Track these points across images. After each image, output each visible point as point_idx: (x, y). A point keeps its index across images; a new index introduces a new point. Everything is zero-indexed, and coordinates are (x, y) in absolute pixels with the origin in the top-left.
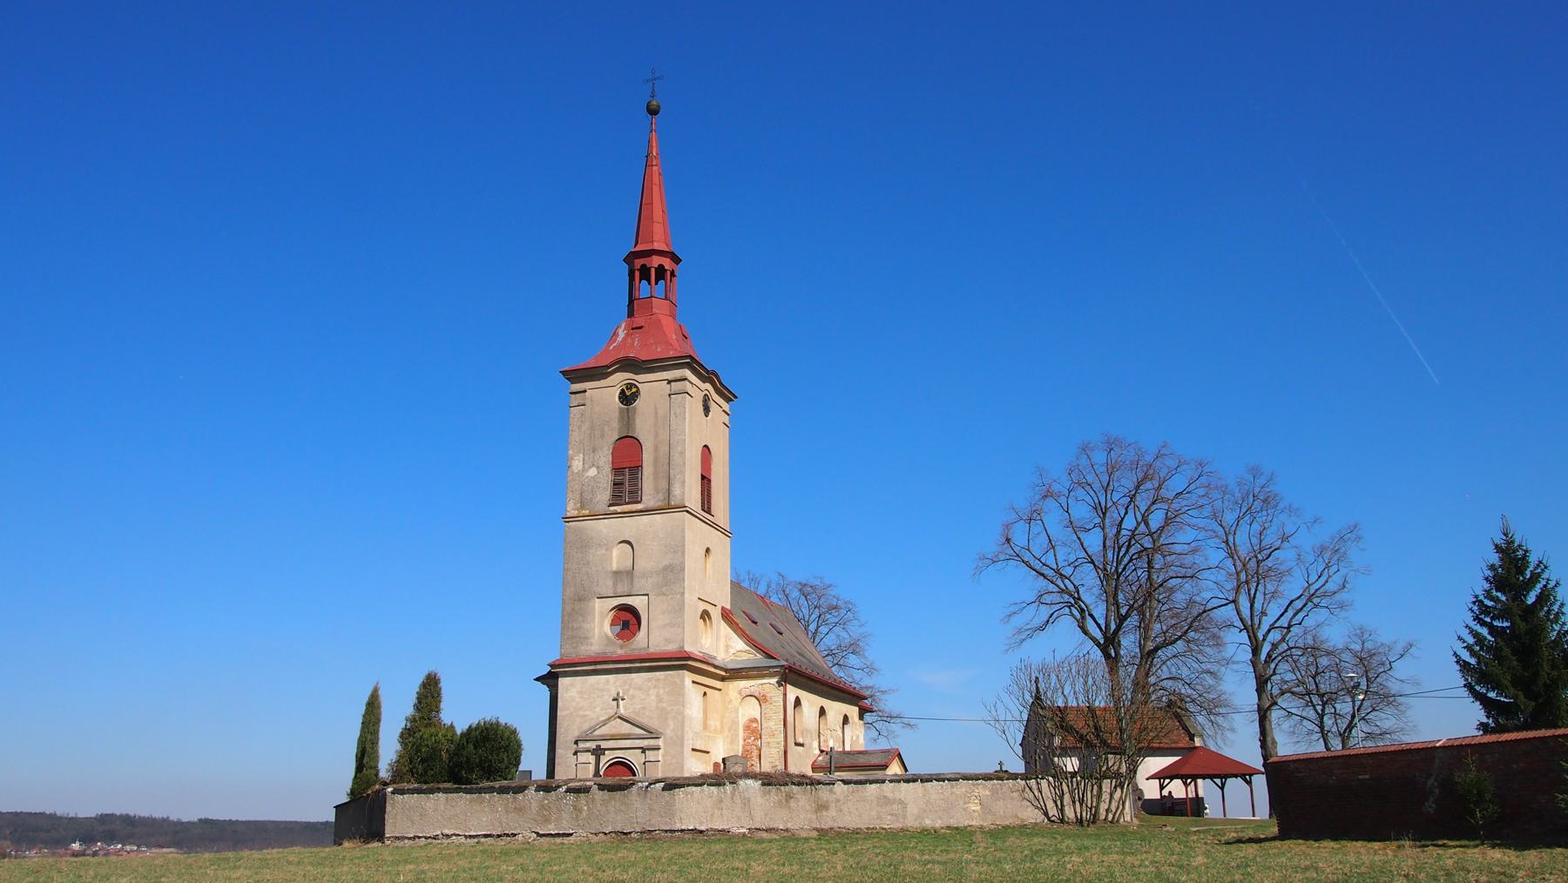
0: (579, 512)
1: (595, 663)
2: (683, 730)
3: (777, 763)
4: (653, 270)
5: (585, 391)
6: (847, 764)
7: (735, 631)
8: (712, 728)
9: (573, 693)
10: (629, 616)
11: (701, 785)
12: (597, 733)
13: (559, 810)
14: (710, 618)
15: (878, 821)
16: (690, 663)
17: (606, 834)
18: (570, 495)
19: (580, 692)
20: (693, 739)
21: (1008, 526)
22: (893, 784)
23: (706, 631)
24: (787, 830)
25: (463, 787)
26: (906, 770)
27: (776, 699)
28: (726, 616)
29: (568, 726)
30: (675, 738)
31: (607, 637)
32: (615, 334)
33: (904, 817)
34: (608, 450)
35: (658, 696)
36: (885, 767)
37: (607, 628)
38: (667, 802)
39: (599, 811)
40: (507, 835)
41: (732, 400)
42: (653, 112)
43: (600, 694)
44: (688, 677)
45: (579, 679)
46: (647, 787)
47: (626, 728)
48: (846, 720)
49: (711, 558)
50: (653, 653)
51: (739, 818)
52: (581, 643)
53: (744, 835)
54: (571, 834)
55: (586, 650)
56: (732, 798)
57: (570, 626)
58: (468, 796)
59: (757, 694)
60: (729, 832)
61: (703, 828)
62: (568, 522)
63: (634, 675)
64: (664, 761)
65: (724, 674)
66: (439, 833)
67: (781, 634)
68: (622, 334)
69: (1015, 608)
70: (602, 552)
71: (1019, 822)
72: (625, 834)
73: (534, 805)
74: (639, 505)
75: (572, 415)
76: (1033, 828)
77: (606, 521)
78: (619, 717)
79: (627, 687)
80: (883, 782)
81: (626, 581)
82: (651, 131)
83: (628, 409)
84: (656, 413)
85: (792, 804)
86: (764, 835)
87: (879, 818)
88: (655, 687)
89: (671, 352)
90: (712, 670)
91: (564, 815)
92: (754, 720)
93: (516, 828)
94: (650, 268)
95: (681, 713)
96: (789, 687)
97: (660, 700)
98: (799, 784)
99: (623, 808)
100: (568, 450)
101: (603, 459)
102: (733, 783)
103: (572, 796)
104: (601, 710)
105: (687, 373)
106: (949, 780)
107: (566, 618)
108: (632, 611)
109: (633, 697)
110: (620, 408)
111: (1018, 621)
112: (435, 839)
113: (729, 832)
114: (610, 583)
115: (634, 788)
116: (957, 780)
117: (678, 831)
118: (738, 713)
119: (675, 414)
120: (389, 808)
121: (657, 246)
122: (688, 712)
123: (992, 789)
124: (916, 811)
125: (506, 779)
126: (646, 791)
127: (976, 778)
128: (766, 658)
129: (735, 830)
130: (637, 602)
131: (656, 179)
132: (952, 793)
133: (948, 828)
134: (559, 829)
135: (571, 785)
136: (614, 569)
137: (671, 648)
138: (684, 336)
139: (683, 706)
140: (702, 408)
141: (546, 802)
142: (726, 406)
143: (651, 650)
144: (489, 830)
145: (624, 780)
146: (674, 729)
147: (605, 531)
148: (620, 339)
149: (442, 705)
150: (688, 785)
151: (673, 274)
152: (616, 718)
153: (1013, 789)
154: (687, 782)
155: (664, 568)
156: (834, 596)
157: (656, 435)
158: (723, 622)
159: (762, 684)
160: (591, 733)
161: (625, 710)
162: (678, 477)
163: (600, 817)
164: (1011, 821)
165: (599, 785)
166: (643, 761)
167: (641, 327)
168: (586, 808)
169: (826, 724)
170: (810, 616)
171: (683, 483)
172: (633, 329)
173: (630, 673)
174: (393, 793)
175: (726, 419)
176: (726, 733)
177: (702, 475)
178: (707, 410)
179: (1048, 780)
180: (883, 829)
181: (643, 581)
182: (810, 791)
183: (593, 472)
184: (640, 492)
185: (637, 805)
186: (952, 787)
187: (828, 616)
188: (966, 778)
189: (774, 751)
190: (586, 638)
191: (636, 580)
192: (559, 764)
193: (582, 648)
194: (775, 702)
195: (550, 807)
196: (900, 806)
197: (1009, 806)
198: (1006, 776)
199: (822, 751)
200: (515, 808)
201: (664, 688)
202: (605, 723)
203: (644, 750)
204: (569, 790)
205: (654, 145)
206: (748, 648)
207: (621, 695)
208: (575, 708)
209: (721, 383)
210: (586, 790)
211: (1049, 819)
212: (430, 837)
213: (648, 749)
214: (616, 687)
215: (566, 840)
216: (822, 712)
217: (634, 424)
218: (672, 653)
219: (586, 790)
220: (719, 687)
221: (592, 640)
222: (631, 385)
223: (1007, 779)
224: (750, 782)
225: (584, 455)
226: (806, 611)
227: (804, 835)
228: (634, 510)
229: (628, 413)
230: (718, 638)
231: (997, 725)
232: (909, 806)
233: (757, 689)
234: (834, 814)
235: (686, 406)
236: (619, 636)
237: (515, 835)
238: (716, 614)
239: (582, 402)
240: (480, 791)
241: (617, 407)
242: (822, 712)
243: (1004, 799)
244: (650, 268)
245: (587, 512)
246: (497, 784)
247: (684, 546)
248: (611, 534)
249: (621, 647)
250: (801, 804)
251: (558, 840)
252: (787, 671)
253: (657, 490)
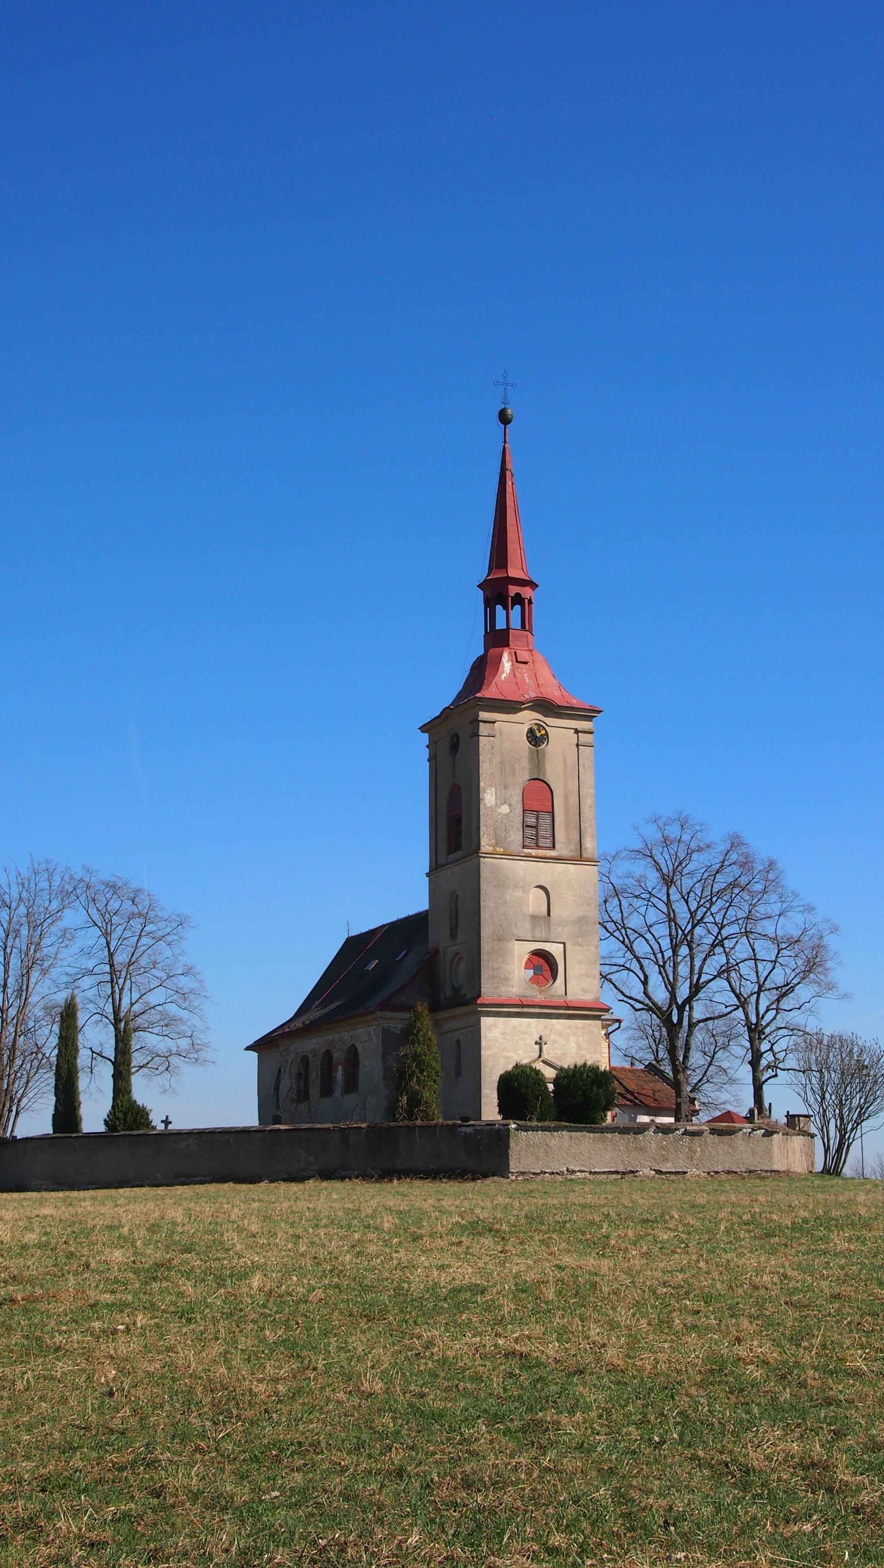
0: (495, 849)
1: (523, 1006)
5: (494, 722)
19: (503, 1033)
29: (493, 1066)
35: (577, 1043)
46: (750, 1133)
52: (502, 983)
55: (507, 992)
57: (491, 965)
58: (591, 1135)
63: (554, 1021)
70: (518, 893)
77: (522, 862)
84: (565, 761)
97: (580, 1048)
103: (687, 1139)
104: (524, 1052)
114: (528, 926)
119: (584, 766)
120: (512, 1144)
126: (749, 1136)
130: (555, 949)
136: (530, 913)
141: (665, 1143)
145: (722, 1126)
147: (521, 873)
168: (699, 1149)
174: (516, 1129)
181: (560, 929)
183: (505, 809)
191: (553, 928)
192: (486, 1104)
193: (503, 989)
200: (636, 1148)
217: (544, 765)
229: (538, 754)
237: (637, 1171)
248: (528, 877)
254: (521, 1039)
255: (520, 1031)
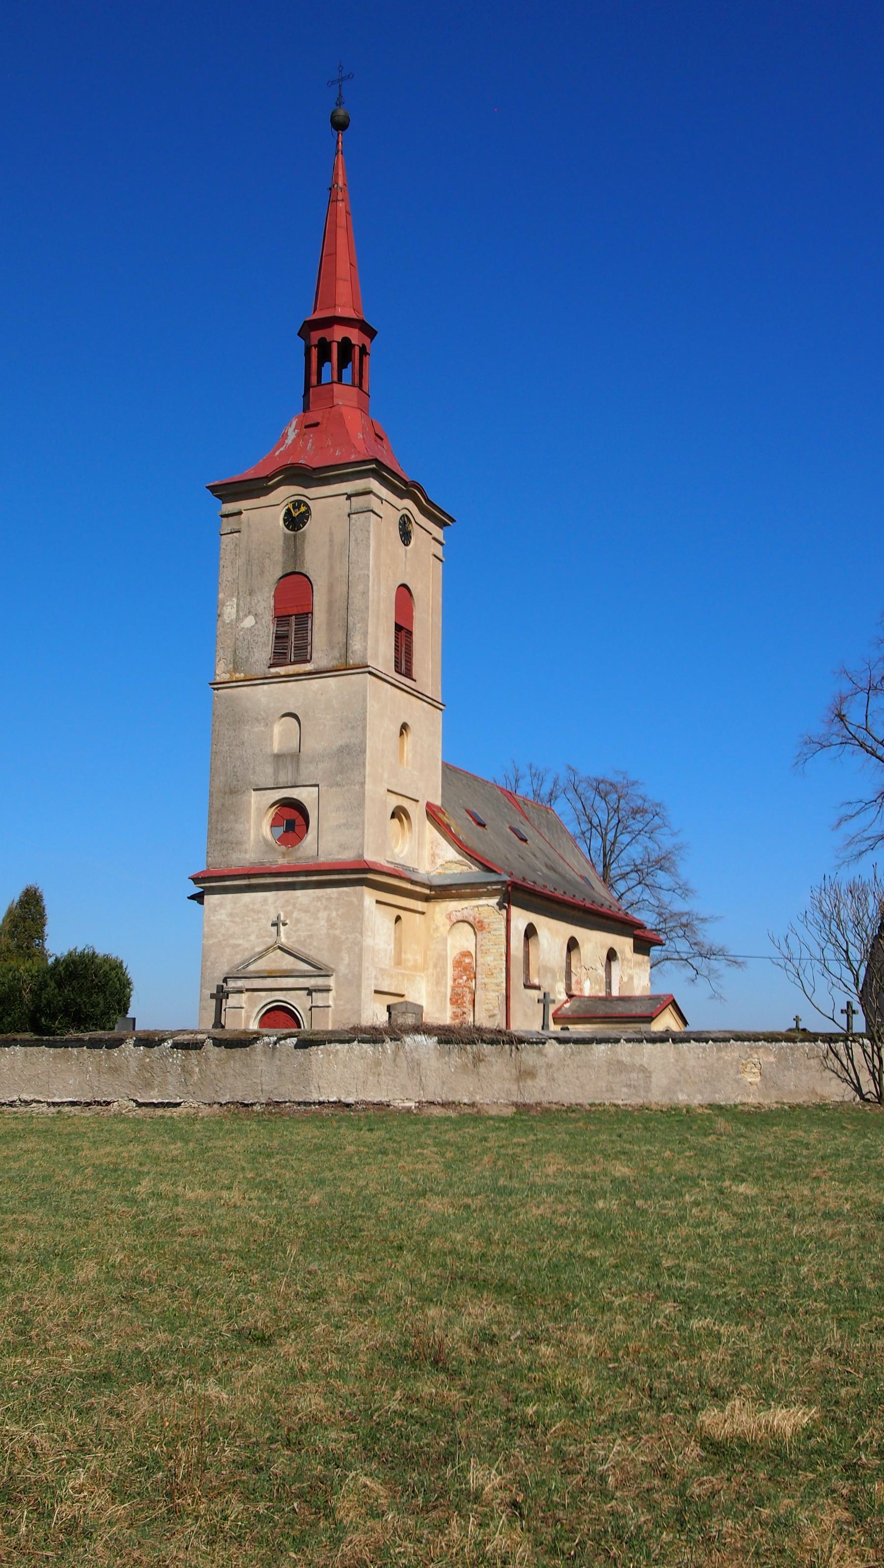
2: (360, 965)
3: (496, 1012)
4: (335, 348)
5: (240, 513)
6: (600, 1013)
7: (444, 835)
8: (410, 964)
9: (222, 915)
10: (294, 814)
11: (349, 1041)
12: (252, 968)
13: (165, 1072)
14: (408, 817)
15: (608, 1095)
16: (370, 876)
17: (221, 1105)
18: (220, 653)
19: (231, 915)
20: (376, 978)
21: (843, 699)
22: (630, 1045)
23: (403, 834)
24: (473, 1105)
25: (45, 1038)
26: (685, 1023)
27: (495, 926)
28: (433, 814)
30: (350, 976)
31: (265, 840)
32: (285, 436)
33: (648, 1090)
34: (270, 592)
35: (329, 920)
36: (649, 1019)
37: (266, 830)
38: (301, 1064)
39: (214, 1074)
40: (99, 1103)
41: (446, 524)
42: (340, 125)
43: (256, 917)
44: (369, 896)
45: (229, 897)
46: (275, 1043)
47: (288, 963)
48: (611, 955)
49: (409, 739)
50: (323, 863)
51: (404, 1087)
52: (233, 849)
53: (409, 1110)
54: (179, 1104)
56: (395, 1060)
57: (219, 827)
58: (52, 1051)
59: (471, 919)
60: (388, 1106)
61: (350, 1100)
62: (218, 689)
63: (299, 893)
64: (335, 1005)
65: (427, 891)
66: (15, 1098)
67: (525, 841)
68: (292, 435)
69: (851, 811)
70: (259, 728)
71: (815, 1100)
72: (246, 1105)
73: (133, 1064)
74: (308, 664)
75: (223, 546)
76: (835, 1109)
77: (265, 687)
78: (280, 948)
79: (290, 908)
80: (617, 1041)
81: (290, 768)
82: (337, 154)
83: (295, 536)
85: (482, 1069)
86: (437, 1111)
87: (610, 1090)
88: (326, 908)
89: (353, 456)
90: (409, 886)
91: (170, 1079)
92: (467, 954)
93: (110, 1093)
94: (331, 342)
95: (358, 944)
96: (514, 910)
97: (332, 925)
98: (492, 1042)
99: (244, 1071)
100: (218, 593)
101: (263, 604)
102: (396, 1040)
103: (179, 1054)
105: (373, 484)
106: (715, 1040)
107: (214, 817)
108: (296, 806)
109: (298, 921)
110: (285, 535)
111: (851, 828)
112: (11, 1106)
113: (388, 1106)
114: (269, 769)
115: (259, 1045)
116: (757, 1040)
117: (314, 1103)
118: (446, 944)
119: (356, 540)
121: (340, 312)
122: (368, 941)
123: (779, 1053)
124: (665, 1082)
125: (103, 1029)
127: (754, 1038)
128: (485, 871)
129: (398, 1104)
131: (342, 220)
132: (718, 1059)
133: (711, 1106)
134: (161, 1096)
135: (180, 1038)
136: (276, 749)
137: (347, 856)
138: (377, 435)
139: (361, 934)
140: (397, 534)
141: (148, 1060)
142: (438, 533)
143: (322, 859)
144: (76, 1096)
146: (349, 964)
147: (264, 700)
148: (289, 441)
149: (47, 929)
150: (330, 1042)
151: (363, 351)
152: (275, 949)
153: (810, 1055)
154: (329, 1037)
155: (339, 750)
156: (641, 797)
157: (332, 569)
158: (428, 823)
159: (477, 907)
160: (244, 968)
161: (288, 938)
162: (359, 625)
163: (215, 1082)
164: (805, 1098)
165: (214, 1039)
166: (309, 1007)
167: (317, 425)
168: (197, 1070)
169: (580, 960)
170: (608, 822)
171: (365, 634)
172: (306, 427)
173: (295, 889)
175: (439, 550)
176: (431, 970)
177: (396, 624)
178: (406, 536)
179: (862, 1046)
180: (615, 1105)
181: (312, 768)
182: (509, 1052)
184: (309, 647)
185: (262, 1067)
186: (719, 1050)
187: (631, 821)
188: (740, 1037)
189: (492, 995)
190: (239, 843)
191: (302, 766)
194: (495, 930)
195: (152, 1068)
196: (641, 1075)
197: (804, 1078)
198: (800, 1036)
199: (571, 996)
200: (110, 1067)
201: (337, 910)
202: (261, 955)
203: (310, 992)
204: (176, 1046)
205: (340, 172)
206: (460, 858)
207: (282, 918)
208: (223, 935)
209: (427, 500)
210: (197, 1046)
211: (862, 1097)
212: (5, 1103)
213: (315, 991)
214: (276, 907)
215: (168, 1112)
216: (573, 945)
218: (350, 863)
219: (197, 1046)
220: (420, 909)
221: (247, 846)
222: (300, 502)
223: (802, 1041)
224: (421, 1038)
225: (238, 599)
226: (604, 817)
227: (493, 1111)
228: (301, 671)
230: (420, 844)
231: (789, 966)
232: (654, 1075)
233: (471, 912)
234: (544, 1084)
235: (372, 529)
236: (282, 840)
238: (417, 812)
239: (236, 528)
240: (66, 1044)
241: (281, 533)
242: (573, 945)
243: (795, 1069)
244: (331, 342)
245: (242, 675)
246: (86, 1036)
247: (365, 719)
249: (284, 855)
250: (495, 1069)
251: (160, 1112)
252: (510, 888)
253: (331, 645)
254: (254, 920)
255: (253, 910)
